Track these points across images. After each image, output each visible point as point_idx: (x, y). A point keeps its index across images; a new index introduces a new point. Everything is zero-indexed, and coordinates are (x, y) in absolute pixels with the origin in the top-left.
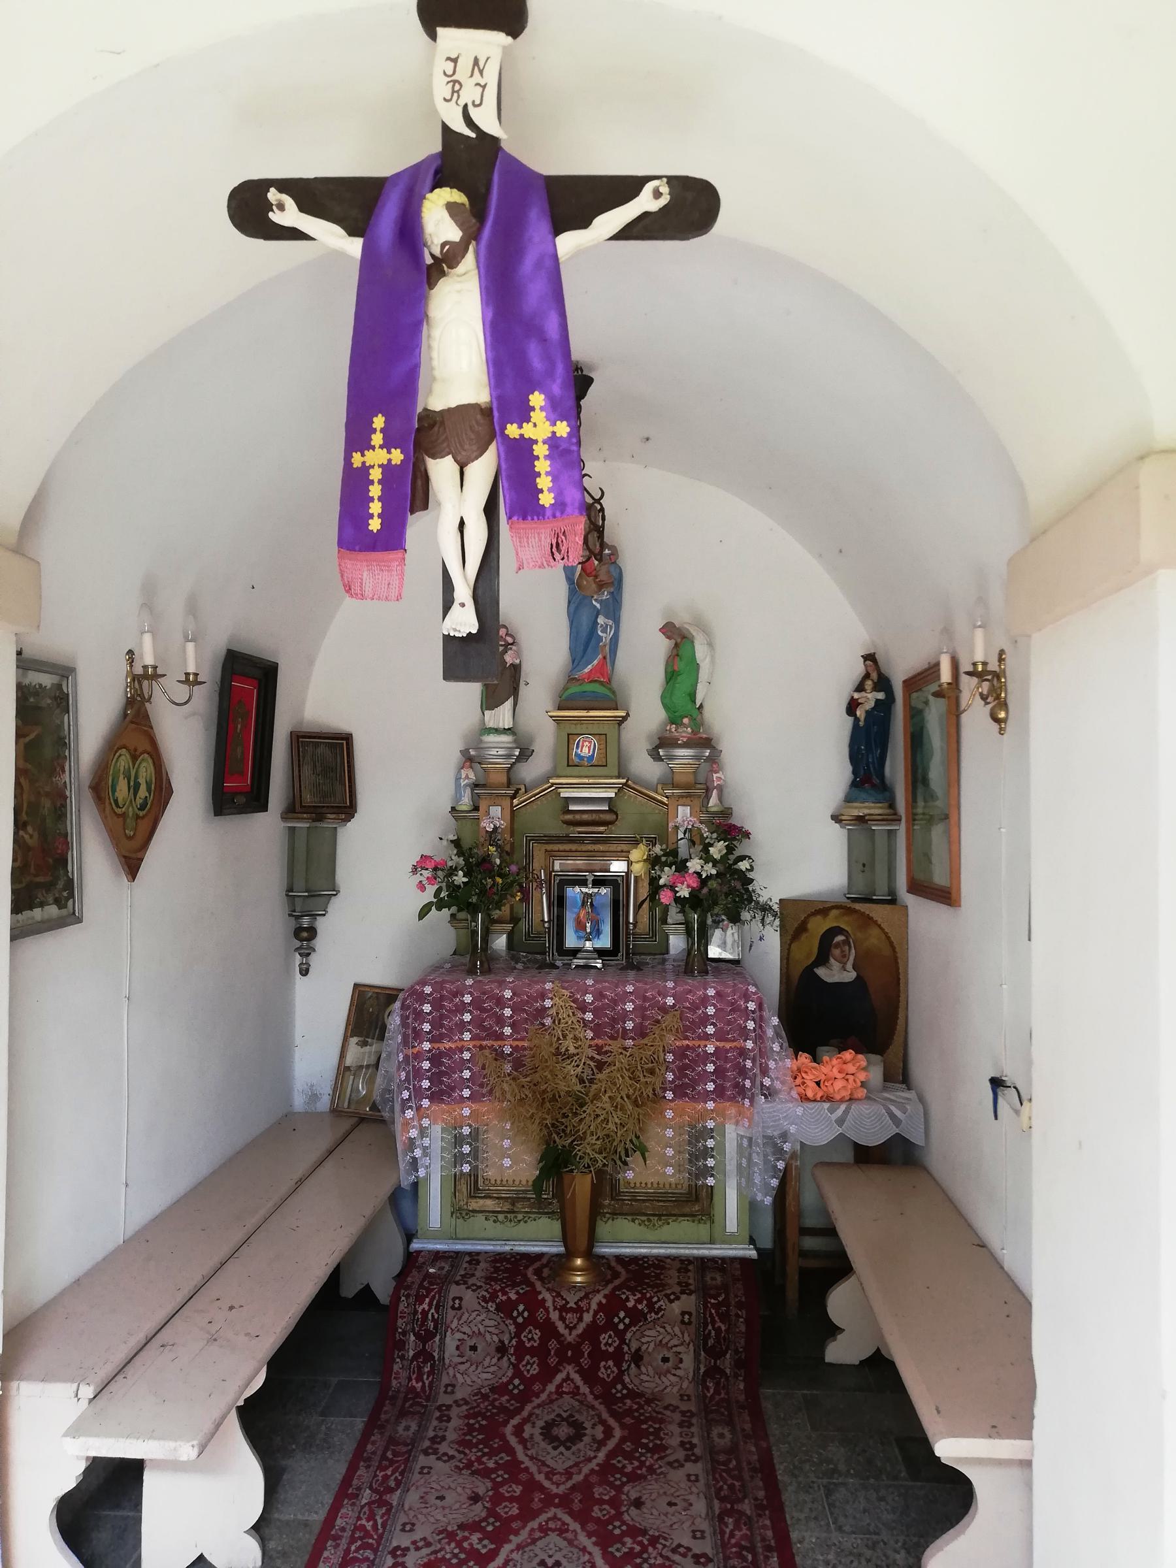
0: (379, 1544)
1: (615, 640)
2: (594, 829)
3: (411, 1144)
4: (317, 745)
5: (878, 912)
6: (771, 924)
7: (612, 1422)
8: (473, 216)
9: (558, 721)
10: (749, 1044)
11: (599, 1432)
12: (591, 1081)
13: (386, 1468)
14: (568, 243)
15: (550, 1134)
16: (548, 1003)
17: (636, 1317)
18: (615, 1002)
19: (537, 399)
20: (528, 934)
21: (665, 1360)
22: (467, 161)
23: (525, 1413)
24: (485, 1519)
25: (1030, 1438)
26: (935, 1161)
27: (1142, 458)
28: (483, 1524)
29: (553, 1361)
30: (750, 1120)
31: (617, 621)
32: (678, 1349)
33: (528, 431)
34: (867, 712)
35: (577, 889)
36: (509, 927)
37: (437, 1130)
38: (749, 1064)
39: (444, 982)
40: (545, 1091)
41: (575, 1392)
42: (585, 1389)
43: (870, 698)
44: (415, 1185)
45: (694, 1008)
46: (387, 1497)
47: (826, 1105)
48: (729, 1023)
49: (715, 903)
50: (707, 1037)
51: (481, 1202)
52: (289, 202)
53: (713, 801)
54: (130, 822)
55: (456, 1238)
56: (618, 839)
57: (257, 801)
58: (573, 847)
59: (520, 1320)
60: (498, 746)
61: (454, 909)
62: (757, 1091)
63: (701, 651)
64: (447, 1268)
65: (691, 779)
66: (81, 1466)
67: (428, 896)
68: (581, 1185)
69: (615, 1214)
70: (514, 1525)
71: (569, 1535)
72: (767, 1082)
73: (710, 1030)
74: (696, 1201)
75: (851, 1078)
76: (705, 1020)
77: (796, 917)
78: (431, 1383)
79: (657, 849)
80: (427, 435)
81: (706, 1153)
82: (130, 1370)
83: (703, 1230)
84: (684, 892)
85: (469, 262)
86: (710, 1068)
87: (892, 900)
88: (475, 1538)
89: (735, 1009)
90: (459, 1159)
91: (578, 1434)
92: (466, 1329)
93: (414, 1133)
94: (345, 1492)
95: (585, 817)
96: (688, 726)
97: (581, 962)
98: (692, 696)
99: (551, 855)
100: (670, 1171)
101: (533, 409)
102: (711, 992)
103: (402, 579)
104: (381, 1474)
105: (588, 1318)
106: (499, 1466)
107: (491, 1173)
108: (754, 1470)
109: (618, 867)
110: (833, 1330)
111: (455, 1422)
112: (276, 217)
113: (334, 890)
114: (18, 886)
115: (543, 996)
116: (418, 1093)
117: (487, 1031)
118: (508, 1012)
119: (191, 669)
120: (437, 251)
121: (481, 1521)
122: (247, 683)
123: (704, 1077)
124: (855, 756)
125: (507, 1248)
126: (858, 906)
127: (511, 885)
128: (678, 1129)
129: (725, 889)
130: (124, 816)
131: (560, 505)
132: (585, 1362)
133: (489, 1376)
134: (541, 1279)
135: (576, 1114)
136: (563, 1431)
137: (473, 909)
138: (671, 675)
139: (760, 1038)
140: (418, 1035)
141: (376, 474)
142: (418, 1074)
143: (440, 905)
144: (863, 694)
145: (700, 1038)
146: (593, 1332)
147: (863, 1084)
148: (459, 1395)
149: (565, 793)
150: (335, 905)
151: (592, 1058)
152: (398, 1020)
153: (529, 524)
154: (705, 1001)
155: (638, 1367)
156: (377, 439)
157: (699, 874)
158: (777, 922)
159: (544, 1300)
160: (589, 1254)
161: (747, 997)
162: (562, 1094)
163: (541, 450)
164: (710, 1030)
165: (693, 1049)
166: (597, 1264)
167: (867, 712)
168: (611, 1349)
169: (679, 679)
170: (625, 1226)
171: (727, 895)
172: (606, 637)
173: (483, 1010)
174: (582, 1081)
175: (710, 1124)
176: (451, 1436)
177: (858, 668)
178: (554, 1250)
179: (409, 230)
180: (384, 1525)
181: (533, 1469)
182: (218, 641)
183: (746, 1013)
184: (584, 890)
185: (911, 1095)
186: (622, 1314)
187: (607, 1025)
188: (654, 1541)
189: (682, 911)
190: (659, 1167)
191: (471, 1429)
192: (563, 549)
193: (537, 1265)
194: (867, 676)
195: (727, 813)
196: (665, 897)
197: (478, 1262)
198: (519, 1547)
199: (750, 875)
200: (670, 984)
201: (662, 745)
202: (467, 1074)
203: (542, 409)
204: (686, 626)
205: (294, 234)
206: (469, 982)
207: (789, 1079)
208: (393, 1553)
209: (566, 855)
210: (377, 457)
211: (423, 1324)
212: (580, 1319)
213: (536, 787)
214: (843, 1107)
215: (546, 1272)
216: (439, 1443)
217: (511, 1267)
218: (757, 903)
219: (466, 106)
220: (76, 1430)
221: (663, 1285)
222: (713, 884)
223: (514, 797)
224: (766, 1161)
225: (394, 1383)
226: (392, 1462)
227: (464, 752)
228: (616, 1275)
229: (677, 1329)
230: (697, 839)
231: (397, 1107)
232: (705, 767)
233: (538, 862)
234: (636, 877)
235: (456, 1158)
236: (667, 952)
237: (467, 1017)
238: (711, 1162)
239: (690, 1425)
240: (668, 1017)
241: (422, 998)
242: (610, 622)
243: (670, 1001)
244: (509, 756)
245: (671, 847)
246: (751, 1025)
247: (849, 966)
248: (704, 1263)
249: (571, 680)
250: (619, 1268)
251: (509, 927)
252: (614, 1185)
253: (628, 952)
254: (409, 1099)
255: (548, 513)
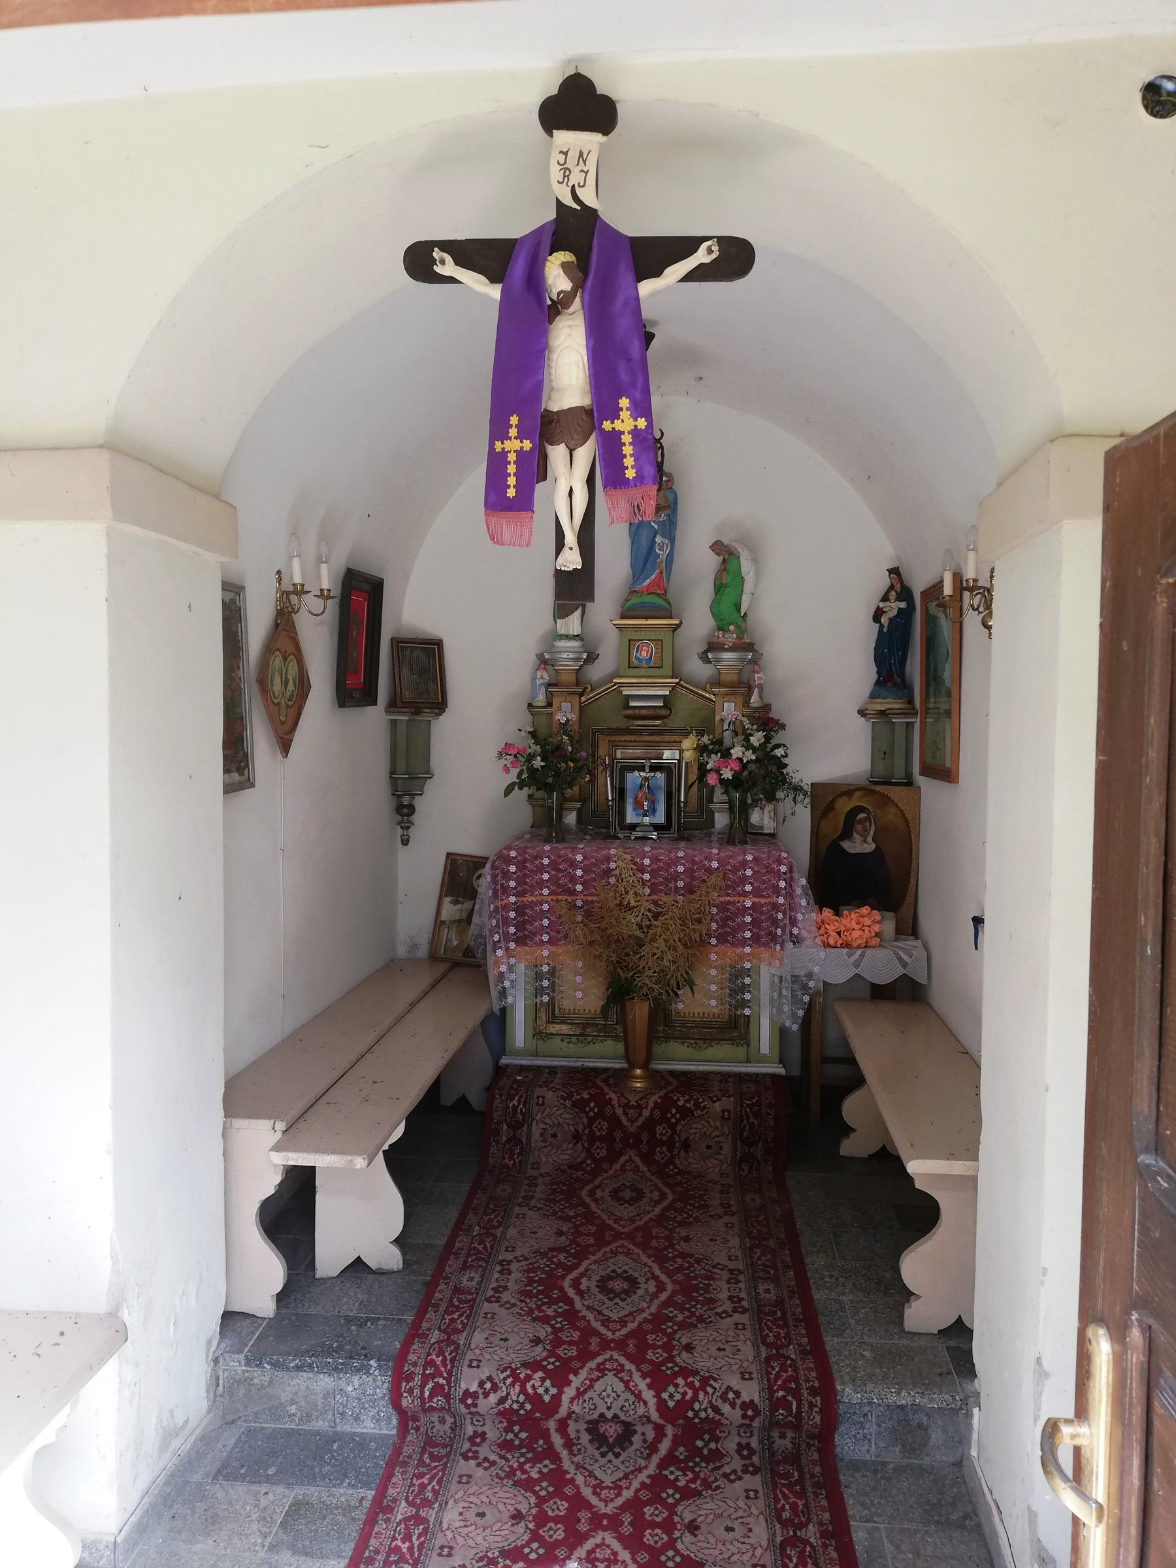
0: (489, 1257)
1: (670, 558)
2: (656, 723)
3: (501, 976)
4: (412, 650)
5: (894, 793)
6: (802, 802)
7: (664, 1278)
8: (579, 271)
9: (620, 628)
10: (781, 900)
11: (656, 1195)
12: (649, 927)
13: (453, 1313)
14: (646, 288)
15: (615, 968)
16: (612, 865)
17: (685, 1113)
18: (669, 865)
19: (624, 402)
20: (594, 812)
21: (708, 1147)
22: (575, 228)
23: (596, 1183)
24: (545, 1359)
25: (971, 1152)
26: (937, 997)
27: (1052, 441)
28: (545, 1363)
29: (618, 1146)
30: (781, 961)
31: (672, 540)
32: (720, 1139)
33: (618, 425)
34: (890, 619)
35: (636, 773)
36: (578, 805)
37: (521, 967)
38: (780, 916)
39: (526, 847)
40: (611, 935)
41: (636, 1170)
42: (644, 1168)
43: (894, 607)
44: (503, 1010)
45: (735, 870)
46: (454, 1337)
47: (845, 950)
48: (764, 882)
49: (755, 784)
50: (745, 894)
51: (558, 1026)
52: (448, 258)
53: (755, 700)
54: (283, 710)
55: (536, 1055)
56: (671, 731)
57: (368, 697)
58: (633, 738)
59: (591, 1114)
60: (568, 651)
61: (533, 788)
62: (786, 937)
63: (746, 566)
64: (531, 1076)
65: (735, 678)
66: (277, 1179)
67: (512, 777)
68: (640, 1011)
69: (668, 1038)
70: (591, 1249)
71: (634, 1257)
72: (795, 931)
73: (748, 888)
74: (735, 1028)
75: (867, 929)
76: (744, 880)
77: (824, 797)
78: (520, 1162)
79: (705, 739)
80: (549, 428)
81: (744, 988)
82: (308, 1116)
83: (741, 1052)
84: (727, 774)
85: (577, 302)
86: (748, 919)
87: (909, 782)
88: (562, 1257)
89: (770, 871)
90: (539, 991)
91: (639, 1195)
92: (548, 1121)
93: (503, 968)
94: (459, 1227)
95: (644, 712)
96: (736, 632)
97: (639, 834)
98: (738, 607)
99: (614, 745)
100: (713, 1003)
101: (621, 409)
102: (749, 857)
103: (530, 532)
104: (448, 1317)
105: (646, 1113)
106: (558, 1314)
107: (566, 1004)
108: (816, 1485)
109: (668, 755)
110: (847, 1130)
111: (516, 1275)
112: (438, 269)
113: (428, 774)
114: (229, 752)
115: (608, 859)
116: (507, 937)
117: (563, 888)
118: (579, 873)
119: (325, 586)
120: (555, 297)
121: (542, 1360)
122: (361, 595)
123: (743, 926)
124: (879, 659)
125: (579, 1064)
126: (878, 788)
127: (581, 769)
128: (721, 968)
129: (763, 772)
130: (278, 705)
131: (640, 478)
132: (644, 1148)
133: (567, 1157)
134: (607, 1084)
135: (636, 953)
136: (627, 1194)
137: (549, 788)
138: (719, 588)
139: (790, 895)
140: (506, 890)
141: (512, 457)
142: (506, 922)
143: (522, 784)
144: (888, 603)
145: (739, 895)
146: (650, 1124)
147: (877, 935)
148: (543, 1170)
149: (626, 692)
150: (430, 787)
151: (650, 910)
152: (489, 878)
153: (618, 492)
154: (744, 864)
155: (687, 1152)
156: (513, 432)
157: (740, 760)
158: (808, 800)
159: (610, 1099)
160: (645, 1066)
161: (779, 862)
162: (625, 937)
163: (627, 438)
164: (748, 888)
165: (733, 903)
166: (656, 1078)
167: (890, 619)
168: (665, 1138)
169: (727, 591)
170: (676, 1048)
171: (764, 778)
172: (662, 554)
173: (559, 871)
174: (641, 928)
175: (747, 965)
176: (538, 1195)
177: (885, 581)
178: (618, 1066)
179: (535, 280)
180: (453, 1360)
181: (604, 1216)
182: (340, 560)
183: (779, 875)
184: (643, 774)
185: (918, 943)
186: (674, 1111)
187: (661, 882)
188: (698, 1261)
189: (726, 792)
190: (704, 999)
191: (530, 1281)
192: (642, 509)
193: (603, 1076)
194: (892, 588)
195: (767, 708)
196: (712, 779)
197: (556, 1073)
198: (595, 1262)
199: (785, 761)
200: (715, 851)
201: (713, 646)
202: (546, 922)
203: (627, 409)
204: (733, 544)
205: (451, 280)
206: (547, 848)
207: (814, 929)
208: (501, 1263)
209: (625, 745)
210: (513, 445)
211: (513, 1116)
212: (640, 1114)
213: (601, 686)
214: (859, 952)
215: (611, 1081)
216: (501, 1292)
217: (584, 1076)
218: (790, 784)
219: (573, 186)
220: (277, 1148)
221: (707, 1207)
222: (752, 767)
223: (581, 695)
224: (794, 996)
225: (491, 1161)
226: (494, 1211)
227: (540, 657)
228: (669, 1084)
229: (718, 1124)
230: (739, 730)
231: (489, 948)
232: (748, 668)
233: (603, 751)
234: (687, 763)
235: (537, 987)
236: (713, 827)
237: (546, 876)
238: (747, 996)
239: (728, 1193)
240: (713, 878)
241: (508, 861)
242: (667, 541)
243: (715, 864)
244: (577, 659)
245: (717, 737)
246: (782, 884)
247: (870, 839)
248: (740, 1078)
249: (633, 592)
250: (671, 1079)
251: (578, 805)
252: (667, 1014)
253: (683, 824)
254: (499, 941)
255: (632, 483)
